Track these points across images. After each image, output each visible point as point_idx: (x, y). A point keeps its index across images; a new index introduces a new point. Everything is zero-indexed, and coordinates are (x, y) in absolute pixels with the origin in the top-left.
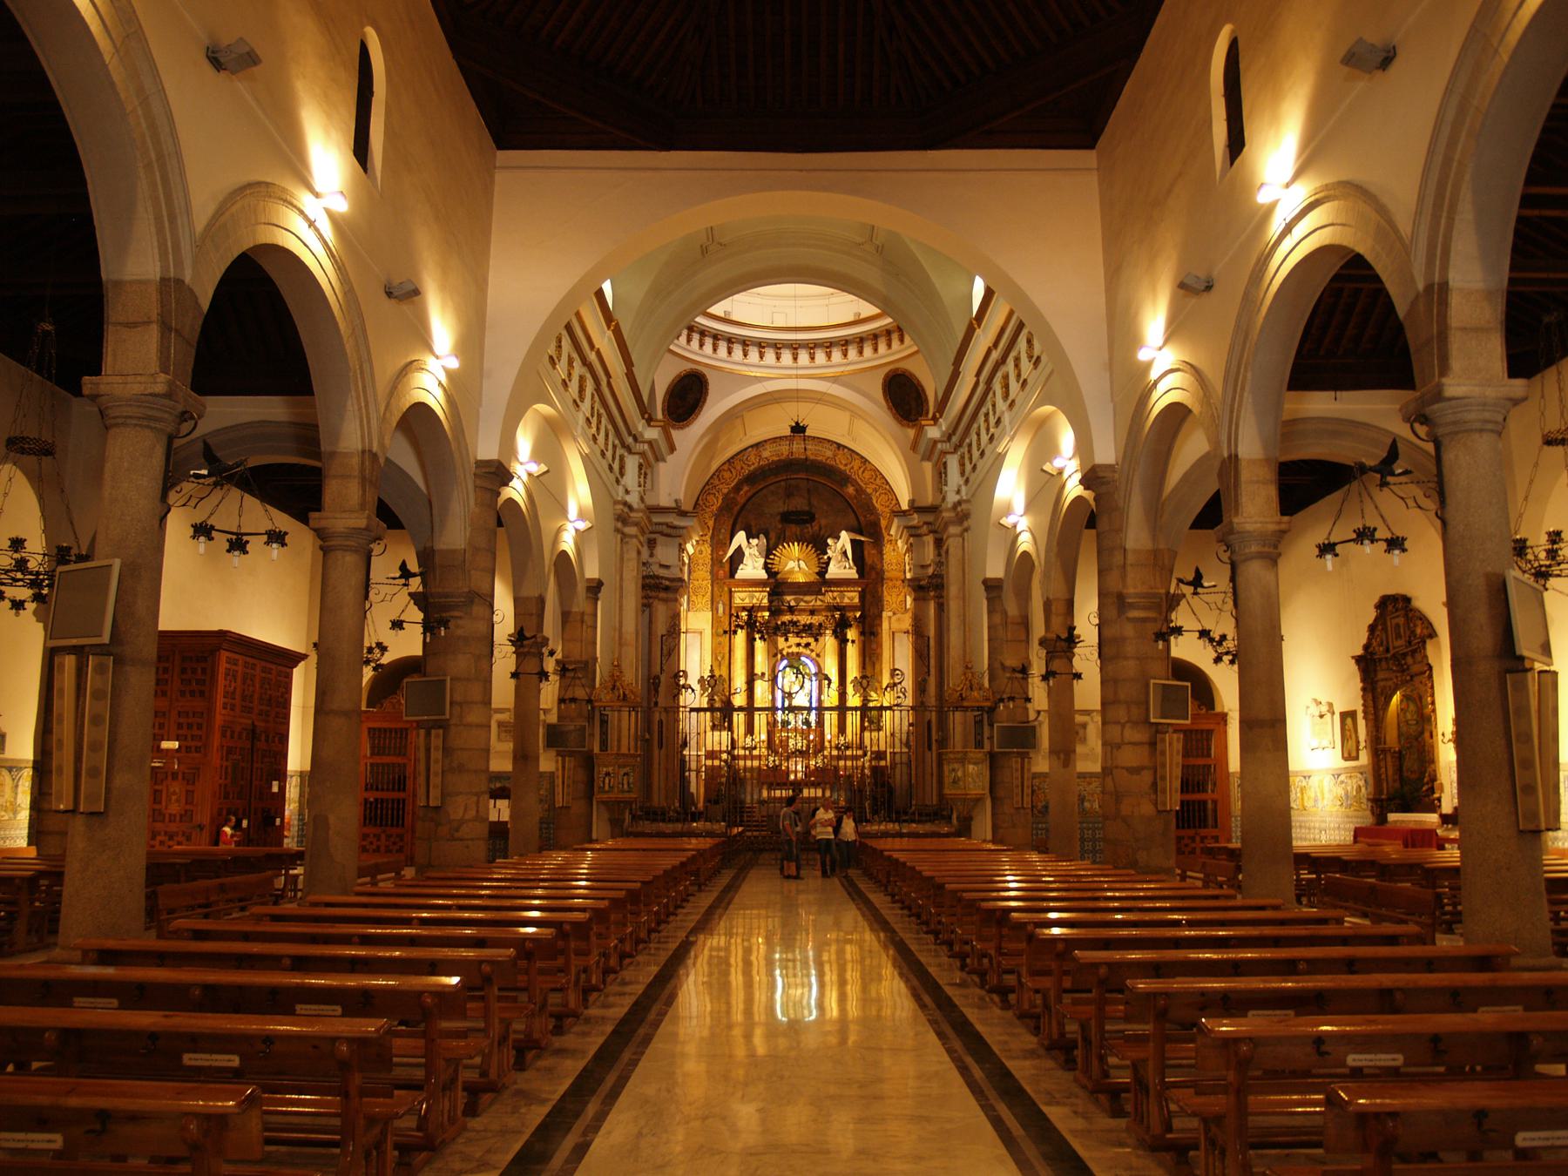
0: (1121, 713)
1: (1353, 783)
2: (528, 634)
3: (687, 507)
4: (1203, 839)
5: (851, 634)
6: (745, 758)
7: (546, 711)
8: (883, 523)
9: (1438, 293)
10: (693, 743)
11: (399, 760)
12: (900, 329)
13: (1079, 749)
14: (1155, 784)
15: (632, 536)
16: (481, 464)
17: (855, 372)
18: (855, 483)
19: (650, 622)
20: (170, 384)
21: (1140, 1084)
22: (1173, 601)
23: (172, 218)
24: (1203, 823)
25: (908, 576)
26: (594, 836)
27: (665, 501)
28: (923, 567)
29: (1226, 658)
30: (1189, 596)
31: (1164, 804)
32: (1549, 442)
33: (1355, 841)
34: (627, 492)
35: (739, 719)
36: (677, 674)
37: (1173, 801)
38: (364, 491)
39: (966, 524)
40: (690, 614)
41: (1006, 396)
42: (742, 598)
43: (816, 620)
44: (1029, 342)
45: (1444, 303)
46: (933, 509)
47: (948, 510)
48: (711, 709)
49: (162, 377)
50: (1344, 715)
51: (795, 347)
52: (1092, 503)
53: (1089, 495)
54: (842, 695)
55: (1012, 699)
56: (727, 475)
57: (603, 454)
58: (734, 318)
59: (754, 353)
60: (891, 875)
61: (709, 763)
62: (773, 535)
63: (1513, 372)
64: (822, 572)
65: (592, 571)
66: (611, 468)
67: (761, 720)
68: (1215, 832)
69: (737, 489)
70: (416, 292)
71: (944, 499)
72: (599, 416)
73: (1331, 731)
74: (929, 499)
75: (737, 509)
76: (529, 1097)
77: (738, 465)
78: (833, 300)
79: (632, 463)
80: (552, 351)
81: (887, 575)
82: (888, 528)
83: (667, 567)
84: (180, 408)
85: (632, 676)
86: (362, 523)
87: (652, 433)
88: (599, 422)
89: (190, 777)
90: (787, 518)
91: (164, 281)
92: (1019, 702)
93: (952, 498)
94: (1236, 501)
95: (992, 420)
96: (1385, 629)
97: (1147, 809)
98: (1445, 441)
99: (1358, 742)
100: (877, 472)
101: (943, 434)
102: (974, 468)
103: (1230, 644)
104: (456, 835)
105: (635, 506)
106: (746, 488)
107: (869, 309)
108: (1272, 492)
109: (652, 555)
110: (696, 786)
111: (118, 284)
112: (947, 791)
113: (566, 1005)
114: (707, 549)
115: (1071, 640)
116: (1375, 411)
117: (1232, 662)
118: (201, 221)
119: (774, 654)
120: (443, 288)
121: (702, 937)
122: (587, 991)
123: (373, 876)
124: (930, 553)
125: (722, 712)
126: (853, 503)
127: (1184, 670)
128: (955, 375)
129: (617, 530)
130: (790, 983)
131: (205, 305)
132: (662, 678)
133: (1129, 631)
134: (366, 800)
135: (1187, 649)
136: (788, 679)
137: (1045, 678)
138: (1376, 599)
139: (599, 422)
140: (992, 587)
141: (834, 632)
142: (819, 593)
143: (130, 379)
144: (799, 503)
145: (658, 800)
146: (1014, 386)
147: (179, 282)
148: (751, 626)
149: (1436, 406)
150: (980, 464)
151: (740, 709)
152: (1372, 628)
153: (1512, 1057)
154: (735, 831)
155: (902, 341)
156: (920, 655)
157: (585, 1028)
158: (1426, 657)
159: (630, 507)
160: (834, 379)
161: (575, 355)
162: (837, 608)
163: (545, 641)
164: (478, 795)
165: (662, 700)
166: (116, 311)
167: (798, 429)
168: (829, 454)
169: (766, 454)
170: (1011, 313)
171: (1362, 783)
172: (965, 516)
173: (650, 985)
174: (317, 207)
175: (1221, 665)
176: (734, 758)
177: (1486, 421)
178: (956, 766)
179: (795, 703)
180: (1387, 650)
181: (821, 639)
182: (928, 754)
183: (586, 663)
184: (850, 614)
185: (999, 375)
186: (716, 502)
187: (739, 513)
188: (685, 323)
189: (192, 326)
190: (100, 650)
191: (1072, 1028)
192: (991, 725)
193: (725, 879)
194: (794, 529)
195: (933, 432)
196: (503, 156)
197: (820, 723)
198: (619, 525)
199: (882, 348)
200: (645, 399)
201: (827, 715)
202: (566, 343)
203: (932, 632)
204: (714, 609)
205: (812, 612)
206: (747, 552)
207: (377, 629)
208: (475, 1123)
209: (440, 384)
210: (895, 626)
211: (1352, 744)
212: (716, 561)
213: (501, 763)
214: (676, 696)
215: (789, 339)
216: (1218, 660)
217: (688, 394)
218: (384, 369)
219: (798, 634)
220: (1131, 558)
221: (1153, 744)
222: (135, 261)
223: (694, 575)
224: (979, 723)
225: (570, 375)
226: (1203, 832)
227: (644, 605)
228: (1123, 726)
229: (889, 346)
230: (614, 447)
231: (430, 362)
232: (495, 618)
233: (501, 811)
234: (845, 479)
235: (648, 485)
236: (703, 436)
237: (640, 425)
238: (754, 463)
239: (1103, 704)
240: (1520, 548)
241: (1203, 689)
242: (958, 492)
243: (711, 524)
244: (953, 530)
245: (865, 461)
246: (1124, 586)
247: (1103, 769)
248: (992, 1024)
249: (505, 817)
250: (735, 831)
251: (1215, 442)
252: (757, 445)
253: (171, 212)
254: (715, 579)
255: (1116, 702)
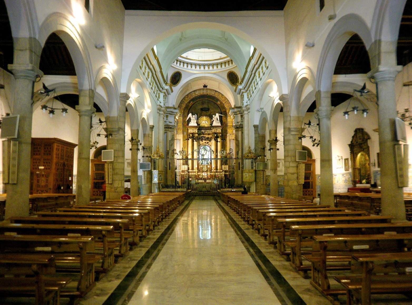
0: (289, 159)
1: (348, 177)
2: (134, 139)
3: (176, 107)
4: (309, 191)
5: (219, 140)
6: (191, 172)
7: (139, 160)
8: (227, 111)
9: (378, 43)
10: (178, 168)
11: (102, 172)
12: (232, 61)
13: (278, 169)
14: (298, 177)
15: (162, 114)
16: (121, 94)
17: (220, 72)
18: (220, 101)
19: (167, 137)
20: (33, 67)
21: (294, 254)
22: (303, 130)
23: (32, 20)
24: (309, 187)
25: (234, 125)
26: (152, 192)
27: (170, 106)
28: (238, 122)
29: (316, 145)
30: (307, 128)
31: (300, 182)
32: (405, 85)
33: (348, 191)
34: (160, 103)
35: (190, 162)
36: (174, 150)
37: (302, 181)
38: (90, 99)
39: (249, 111)
40: (177, 135)
41: (259, 77)
42: (190, 131)
43: (210, 136)
44: (265, 62)
45: (380, 46)
46: (240, 107)
47: (244, 107)
48: (183, 159)
49: (30, 65)
50: (345, 160)
51: (204, 65)
52: (282, 104)
53: (281, 102)
54: (217, 156)
55: (261, 156)
56: (186, 99)
57: (154, 93)
58: (189, 58)
59: (194, 67)
60: (228, 201)
61: (182, 173)
62: (199, 114)
63: (399, 63)
64: (211, 124)
65: (151, 123)
66: (156, 96)
67: (195, 162)
68: (312, 190)
69: (189, 102)
70: (103, 47)
71: (243, 104)
72: (153, 82)
73: (342, 164)
74: (239, 105)
75: (189, 107)
76: (132, 260)
77: (189, 96)
78: (214, 53)
79: (162, 95)
80: (140, 64)
81: (228, 125)
82: (229, 112)
83: (171, 122)
84: (36, 74)
85: (162, 151)
86: (89, 108)
87: (167, 87)
88: (153, 84)
89: (47, 176)
90: (202, 110)
91: (30, 38)
92: (262, 157)
93: (245, 104)
94: (320, 102)
95: (256, 83)
96: (356, 137)
97: (296, 184)
98: (379, 83)
99: (349, 166)
100: (226, 98)
101: (243, 87)
102: (251, 96)
103: (316, 141)
104: (116, 191)
105: (163, 106)
106: (191, 102)
107: (224, 55)
108: (329, 100)
109: (167, 119)
110: (178, 179)
111: (17, 39)
112: (244, 180)
113: (142, 234)
114: (181, 118)
115: (276, 140)
116: (354, 80)
117: (317, 146)
118: (41, 22)
119: (199, 146)
120: (111, 47)
121: (180, 217)
122: (148, 231)
123: (95, 201)
124: (239, 119)
125: (186, 161)
126: (220, 106)
127: (304, 148)
128: (246, 72)
129: (158, 113)
130: (202, 226)
131: (43, 45)
132: (169, 153)
133: (291, 137)
134: (94, 182)
135: (306, 142)
136: (202, 152)
137: (270, 150)
138: (354, 129)
139: (153, 84)
140: (256, 127)
141: (215, 139)
142: (211, 129)
143: (21, 65)
144: (205, 106)
145: (169, 183)
146: (261, 74)
147: (35, 39)
148: (193, 138)
149: (377, 73)
150: (259, 83)
151: (190, 159)
152: (353, 137)
153: (398, 246)
154: (189, 191)
155: (232, 64)
156: (237, 145)
157: (147, 240)
158: (367, 144)
159: (161, 107)
160: (215, 74)
161: (147, 66)
162: (215, 133)
163: (139, 141)
164: (122, 181)
165: (170, 156)
166: (17, 46)
167: (205, 86)
168: (213, 93)
169: (197, 93)
170: (261, 54)
171: (350, 177)
172: (249, 109)
173: (166, 229)
174: (75, 23)
175: (314, 147)
176: (189, 172)
177: (391, 77)
178: (247, 174)
179: (205, 157)
180: (357, 143)
181: (211, 141)
182: (239, 171)
183: (150, 147)
184: (219, 135)
185: (258, 71)
186: (184, 106)
187: (189, 109)
188: (176, 58)
189: (39, 52)
190: (14, 139)
191: (276, 238)
192: (255, 163)
193: (186, 202)
194: (204, 112)
195: (240, 87)
196: (127, 12)
197: (211, 163)
198: (158, 111)
199: (227, 65)
200: (165, 78)
201: (213, 161)
202: (144, 63)
203: (240, 139)
204: (183, 134)
205: (209, 134)
206: (192, 119)
207: (94, 138)
208: (117, 265)
209: (111, 73)
210: (230, 138)
211: (347, 167)
212: (184, 121)
213: (128, 172)
214: (173, 156)
215: (202, 63)
216: (314, 145)
217: (176, 78)
218: (95, 67)
219: (205, 140)
220: (292, 119)
221: (297, 167)
222: (21, 32)
223: (178, 125)
224: (252, 162)
225: (145, 71)
226: (309, 190)
227: (165, 132)
228: (290, 162)
229: (229, 65)
230: (157, 91)
231: (107, 65)
232: (126, 135)
233: (127, 185)
234: (218, 100)
235: (166, 101)
236: (181, 87)
237: (164, 85)
238: (194, 95)
239: (285, 157)
240: (398, 112)
241: (310, 154)
242: (247, 103)
243: (182, 111)
244: (245, 112)
245: (222, 95)
246: (290, 126)
247: (285, 173)
248: (256, 238)
249: (129, 187)
250: (189, 191)
251: (314, 88)
252: (194, 91)
253: (31, 19)
254: (183, 125)
255: (288, 156)
